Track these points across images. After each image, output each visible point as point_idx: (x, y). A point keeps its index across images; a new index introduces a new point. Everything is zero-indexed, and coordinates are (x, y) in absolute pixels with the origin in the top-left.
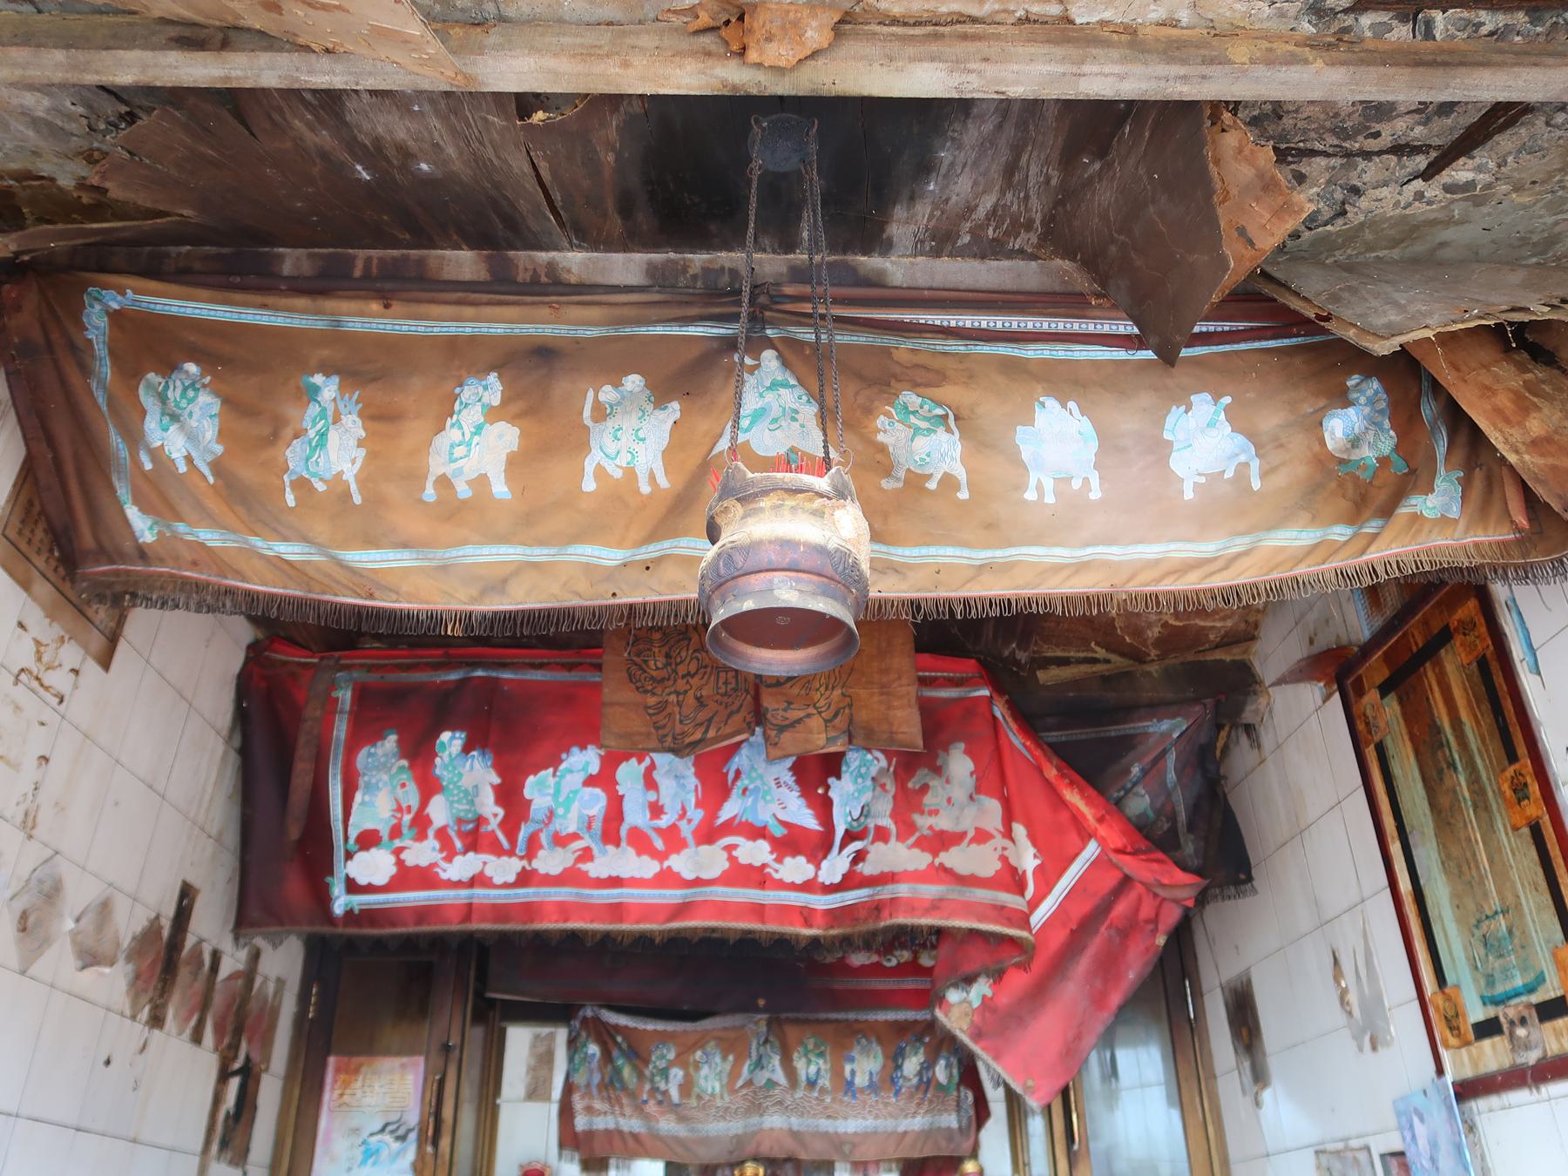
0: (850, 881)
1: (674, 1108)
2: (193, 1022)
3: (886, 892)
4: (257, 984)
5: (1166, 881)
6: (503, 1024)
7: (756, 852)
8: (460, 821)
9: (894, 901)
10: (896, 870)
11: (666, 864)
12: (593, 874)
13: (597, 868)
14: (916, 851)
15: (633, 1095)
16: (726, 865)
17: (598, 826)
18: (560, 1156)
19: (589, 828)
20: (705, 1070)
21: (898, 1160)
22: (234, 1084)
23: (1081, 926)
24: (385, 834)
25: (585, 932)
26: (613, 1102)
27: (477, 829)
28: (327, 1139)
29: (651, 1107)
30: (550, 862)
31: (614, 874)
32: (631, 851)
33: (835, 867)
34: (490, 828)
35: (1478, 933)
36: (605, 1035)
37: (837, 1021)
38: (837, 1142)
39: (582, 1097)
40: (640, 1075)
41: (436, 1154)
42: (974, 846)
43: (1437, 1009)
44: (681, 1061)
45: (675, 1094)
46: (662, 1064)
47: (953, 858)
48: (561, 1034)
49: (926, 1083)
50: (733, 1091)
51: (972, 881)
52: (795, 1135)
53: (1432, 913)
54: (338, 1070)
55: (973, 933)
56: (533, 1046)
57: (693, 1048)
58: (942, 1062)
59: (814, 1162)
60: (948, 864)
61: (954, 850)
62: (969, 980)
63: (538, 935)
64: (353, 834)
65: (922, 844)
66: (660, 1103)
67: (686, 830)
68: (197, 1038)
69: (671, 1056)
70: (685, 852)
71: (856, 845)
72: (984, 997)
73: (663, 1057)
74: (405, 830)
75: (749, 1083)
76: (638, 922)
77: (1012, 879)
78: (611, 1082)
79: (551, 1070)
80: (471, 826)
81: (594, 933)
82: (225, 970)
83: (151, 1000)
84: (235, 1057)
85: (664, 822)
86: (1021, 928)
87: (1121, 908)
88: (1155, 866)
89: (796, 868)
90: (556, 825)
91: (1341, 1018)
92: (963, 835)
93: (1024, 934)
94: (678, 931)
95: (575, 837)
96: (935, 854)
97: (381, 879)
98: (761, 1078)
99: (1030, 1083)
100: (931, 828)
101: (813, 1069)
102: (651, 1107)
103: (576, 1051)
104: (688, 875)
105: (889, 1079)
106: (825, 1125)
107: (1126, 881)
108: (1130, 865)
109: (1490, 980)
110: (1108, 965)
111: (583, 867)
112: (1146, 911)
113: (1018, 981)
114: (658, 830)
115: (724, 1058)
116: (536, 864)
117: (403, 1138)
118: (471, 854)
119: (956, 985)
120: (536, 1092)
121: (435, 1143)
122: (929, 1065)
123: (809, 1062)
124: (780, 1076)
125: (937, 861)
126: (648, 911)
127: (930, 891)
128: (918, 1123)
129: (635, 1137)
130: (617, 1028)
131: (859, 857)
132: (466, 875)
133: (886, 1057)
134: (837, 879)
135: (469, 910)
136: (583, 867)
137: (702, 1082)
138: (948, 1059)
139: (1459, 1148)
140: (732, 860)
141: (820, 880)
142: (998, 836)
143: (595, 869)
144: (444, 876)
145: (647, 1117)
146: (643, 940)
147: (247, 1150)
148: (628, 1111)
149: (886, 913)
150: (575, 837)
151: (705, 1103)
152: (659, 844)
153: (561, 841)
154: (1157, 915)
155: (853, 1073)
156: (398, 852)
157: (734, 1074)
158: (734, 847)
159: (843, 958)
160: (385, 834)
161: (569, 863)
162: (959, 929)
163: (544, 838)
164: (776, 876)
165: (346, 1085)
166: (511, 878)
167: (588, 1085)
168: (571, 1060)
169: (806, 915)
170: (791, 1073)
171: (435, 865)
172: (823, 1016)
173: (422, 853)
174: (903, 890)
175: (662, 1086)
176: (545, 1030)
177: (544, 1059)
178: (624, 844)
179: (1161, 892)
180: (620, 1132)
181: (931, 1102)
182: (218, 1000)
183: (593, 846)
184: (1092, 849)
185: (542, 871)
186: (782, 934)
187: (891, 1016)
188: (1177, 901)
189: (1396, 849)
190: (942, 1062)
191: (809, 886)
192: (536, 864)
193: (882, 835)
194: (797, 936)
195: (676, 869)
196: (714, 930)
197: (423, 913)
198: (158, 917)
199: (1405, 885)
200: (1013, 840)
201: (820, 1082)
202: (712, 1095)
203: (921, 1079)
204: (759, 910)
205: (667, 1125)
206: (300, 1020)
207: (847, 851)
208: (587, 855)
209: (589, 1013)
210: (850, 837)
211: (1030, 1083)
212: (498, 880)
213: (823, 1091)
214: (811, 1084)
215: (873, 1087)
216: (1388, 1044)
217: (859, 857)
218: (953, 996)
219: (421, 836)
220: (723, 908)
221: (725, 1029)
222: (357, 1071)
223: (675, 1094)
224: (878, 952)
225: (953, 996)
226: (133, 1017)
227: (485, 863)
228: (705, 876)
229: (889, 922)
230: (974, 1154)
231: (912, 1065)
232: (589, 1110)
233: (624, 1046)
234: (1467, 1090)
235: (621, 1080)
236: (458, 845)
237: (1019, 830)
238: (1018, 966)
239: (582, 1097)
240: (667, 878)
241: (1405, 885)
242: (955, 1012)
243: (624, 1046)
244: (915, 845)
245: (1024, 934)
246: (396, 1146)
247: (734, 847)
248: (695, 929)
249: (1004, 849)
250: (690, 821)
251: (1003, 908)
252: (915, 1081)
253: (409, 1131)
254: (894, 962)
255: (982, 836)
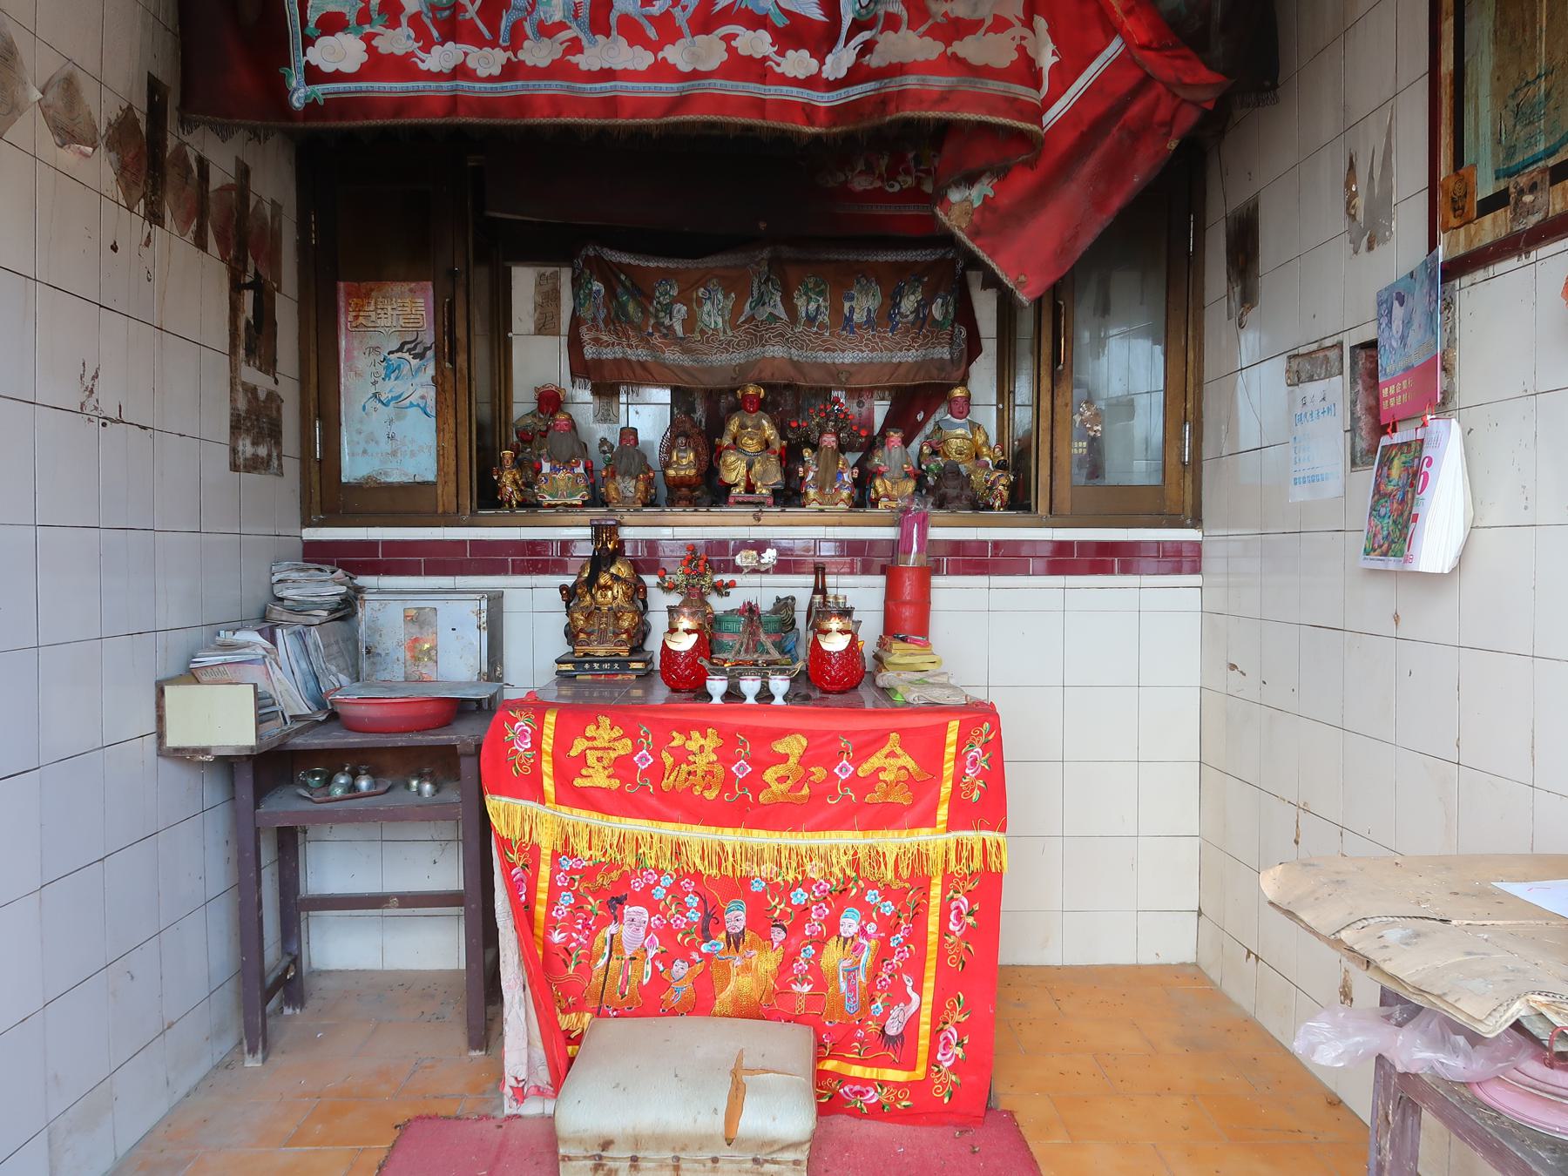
0: (856, 74)
1: (678, 341)
2: (193, 227)
3: (893, 85)
4: (252, 204)
5: (1188, 80)
6: (508, 264)
7: (757, 43)
8: (434, 8)
9: (902, 94)
10: (905, 60)
11: (660, 55)
12: (583, 67)
13: (587, 61)
14: (928, 39)
15: (639, 329)
16: (725, 56)
17: (585, 12)
18: (573, 383)
19: (576, 16)
20: (708, 307)
21: (890, 388)
22: (248, 297)
23: (1091, 125)
24: (352, 18)
25: (579, 127)
26: (621, 334)
27: (454, 16)
28: (348, 358)
29: (657, 340)
30: (537, 53)
31: (606, 66)
32: (623, 42)
33: (840, 61)
34: (468, 16)
35: (1512, 104)
36: (608, 273)
37: (837, 261)
38: (834, 372)
39: (589, 329)
40: (645, 311)
41: (454, 370)
42: (991, 35)
43: (1446, 193)
44: (684, 298)
45: (679, 329)
46: (665, 300)
47: (970, 49)
48: (566, 275)
49: (922, 318)
50: (734, 327)
51: (987, 72)
52: (796, 365)
53: (1469, 90)
54: (349, 295)
55: (982, 126)
56: (538, 285)
57: (695, 285)
58: (939, 301)
59: (812, 388)
60: (961, 54)
61: (969, 39)
62: (970, 180)
63: (531, 129)
64: (313, 17)
65: (933, 33)
66: (665, 336)
67: (681, 18)
68: (201, 244)
69: (674, 292)
70: (680, 42)
71: (865, 35)
72: (986, 196)
73: (667, 293)
74: (375, 16)
75: (752, 318)
76: (633, 117)
77: (1026, 70)
78: (617, 316)
79: (558, 306)
80: (447, 13)
81: (589, 127)
82: (216, 180)
83: (144, 196)
84: (245, 271)
85: (656, 10)
86: (1032, 123)
87: (1136, 109)
88: (1179, 63)
89: (798, 63)
90: (540, 13)
91: (1342, 224)
92: (981, 22)
93: (1036, 128)
94: (677, 125)
95: (562, 26)
96: (948, 44)
97: (350, 66)
98: (763, 313)
99: (1022, 278)
100: (945, 15)
101: (813, 306)
102: (657, 340)
103: (580, 287)
104: (685, 67)
105: (886, 317)
106: (824, 357)
107: (1147, 81)
108: (1154, 63)
109: (1511, 152)
110: (1113, 169)
111: (574, 59)
112: (1162, 113)
113: (1023, 181)
114: (650, 18)
115: (726, 296)
116: (522, 55)
117: (421, 356)
118: (450, 45)
119: (957, 184)
120: (545, 327)
121: (453, 361)
122: (925, 303)
123: (809, 300)
124: (780, 311)
125: (949, 51)
126: (643, 105)
127: (939, 82)
128: (911, 356)
129: (642, 364)
130: (619, 265)
131: (867, 47)
132: (447, 66)
133: (884, 296)
134: (842, 73)
135: (454, 102)
136: (574, 59)
137: (705, 317)
138: (944, 298)
139: (1431, 316)
140: (731, 50)
141: (824, 75)
142: (1018, 24)
143: (586, 61)
144: (423, 67)
145: (652, 348)
146: (638, 134)
147: (275, 361)
148: (634, 342)
149: (893, 106)
150: (562, 26)
151: (708, 337)
152: (652, 33)
153: (547, 31)
154: (1173, 118)
155: (852, 310)
156: (368, 39)
157: (736, 311)
158: (734, 36)
159: (846, 182)
160: (352, 18)
161: (558, 56)
162: (968, 122)
163: (528, 28)
164: (778, 70)
165: (359, 308)
166: (496, 71)
167: (594, 319)
168: (576, 296)
169: (809, 112)
170: (791, 310)
171: (412, 54)
172: (824, 256)
173: (397, 41)
174: (911, 81)
175: (667, 322)
176: (549, 270)
177: (549, 298)
178: (614, 33)
179: (1182, 94)
180: (629, 362)
181: (925, 337)
182: (213, 208)
183: (582, 36)
184: (1115, 47)
185: (529, 63)
186: (784, 131)
187: (891, 257)
188: (1195, 103)
189: (1448, 27)
190: (939, 301)
191: (812, 82)
192: (522, 55)
193: (892, 23)
194: (799, 133)
195: (671, 60)
196: (713, 125)
197: (402, 105)
198: (130, 107)
199: (1447, 65)
200: (1033, 30)
201: (820, 318)
202: (715, 329)
203: (917, 316)
204: (759, 105)
205: (672, 356)
206: (303, 248)
207: (852, 43)
208: (575, 46)
209: (591, 253)
210: (857, 26)
211: (1022, 278)
212: (482, 73)
213: (822, 326)
214: (811, 320)
215: (870, 323)
216: (1385, 240)
217: (867, 47)
218: (955, 196)
219: (394, 23)
220: (722, 102)
221: (726, 267)
222: (368, 295)
223: (679, 329)
224: (881, 177)
225: (955, 196)
226: (130, 210)
227: (466, 54)
228: (702, 68)
229: (894, 116)
230: (964, 382)
231: (908, 304)
232: (597, 341)
233: (628, 284)
234: (1456, 268)
235: (626, 314)
236: (435, 34)
237: (1041, 23)
238: (1025, 164)
239: (589, 329)
240: (662, 71)
241: (1447, 65)
242: (955, 211)
243: (628, 284)
244: (926, 34)
245: (1036, 128)
246: (415, 362)
247: (734, 36)
248: (694, 123)
249: (1023, 38)
250: (684, 8)
251: (1016, 100)
252: (911, 317)
253: (427, 349)
254: (897, 188)
255: (1000, 25)
